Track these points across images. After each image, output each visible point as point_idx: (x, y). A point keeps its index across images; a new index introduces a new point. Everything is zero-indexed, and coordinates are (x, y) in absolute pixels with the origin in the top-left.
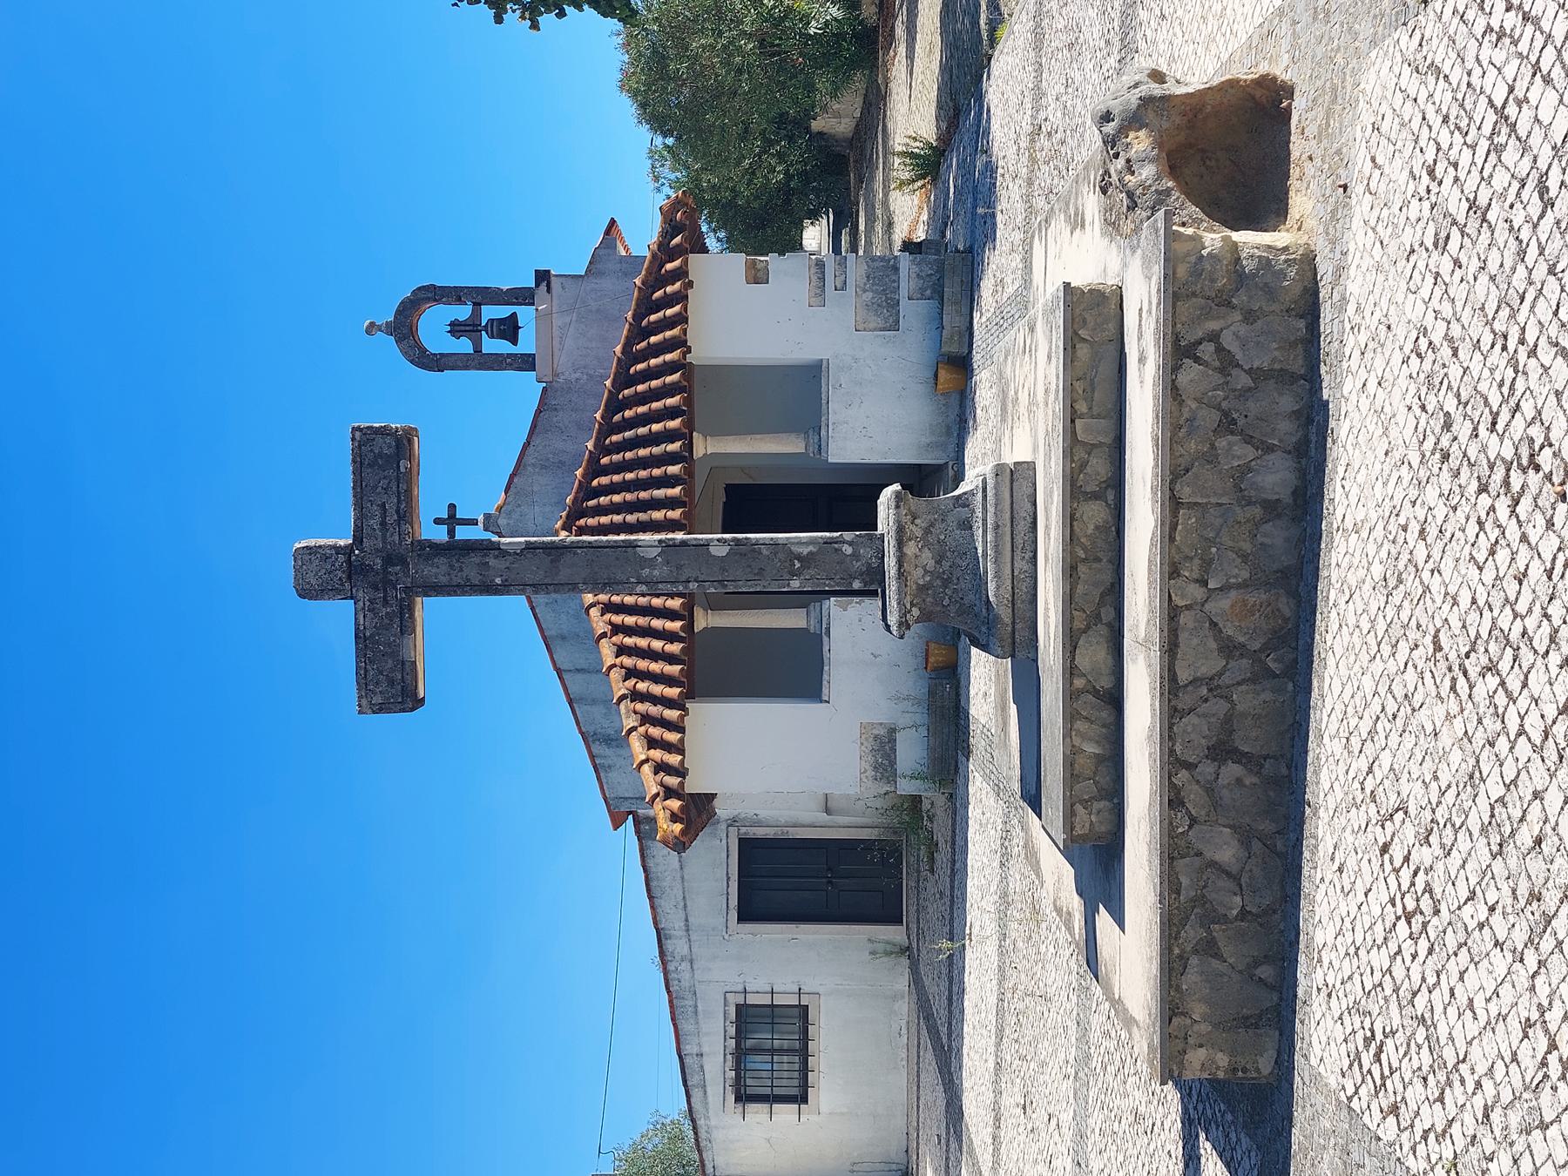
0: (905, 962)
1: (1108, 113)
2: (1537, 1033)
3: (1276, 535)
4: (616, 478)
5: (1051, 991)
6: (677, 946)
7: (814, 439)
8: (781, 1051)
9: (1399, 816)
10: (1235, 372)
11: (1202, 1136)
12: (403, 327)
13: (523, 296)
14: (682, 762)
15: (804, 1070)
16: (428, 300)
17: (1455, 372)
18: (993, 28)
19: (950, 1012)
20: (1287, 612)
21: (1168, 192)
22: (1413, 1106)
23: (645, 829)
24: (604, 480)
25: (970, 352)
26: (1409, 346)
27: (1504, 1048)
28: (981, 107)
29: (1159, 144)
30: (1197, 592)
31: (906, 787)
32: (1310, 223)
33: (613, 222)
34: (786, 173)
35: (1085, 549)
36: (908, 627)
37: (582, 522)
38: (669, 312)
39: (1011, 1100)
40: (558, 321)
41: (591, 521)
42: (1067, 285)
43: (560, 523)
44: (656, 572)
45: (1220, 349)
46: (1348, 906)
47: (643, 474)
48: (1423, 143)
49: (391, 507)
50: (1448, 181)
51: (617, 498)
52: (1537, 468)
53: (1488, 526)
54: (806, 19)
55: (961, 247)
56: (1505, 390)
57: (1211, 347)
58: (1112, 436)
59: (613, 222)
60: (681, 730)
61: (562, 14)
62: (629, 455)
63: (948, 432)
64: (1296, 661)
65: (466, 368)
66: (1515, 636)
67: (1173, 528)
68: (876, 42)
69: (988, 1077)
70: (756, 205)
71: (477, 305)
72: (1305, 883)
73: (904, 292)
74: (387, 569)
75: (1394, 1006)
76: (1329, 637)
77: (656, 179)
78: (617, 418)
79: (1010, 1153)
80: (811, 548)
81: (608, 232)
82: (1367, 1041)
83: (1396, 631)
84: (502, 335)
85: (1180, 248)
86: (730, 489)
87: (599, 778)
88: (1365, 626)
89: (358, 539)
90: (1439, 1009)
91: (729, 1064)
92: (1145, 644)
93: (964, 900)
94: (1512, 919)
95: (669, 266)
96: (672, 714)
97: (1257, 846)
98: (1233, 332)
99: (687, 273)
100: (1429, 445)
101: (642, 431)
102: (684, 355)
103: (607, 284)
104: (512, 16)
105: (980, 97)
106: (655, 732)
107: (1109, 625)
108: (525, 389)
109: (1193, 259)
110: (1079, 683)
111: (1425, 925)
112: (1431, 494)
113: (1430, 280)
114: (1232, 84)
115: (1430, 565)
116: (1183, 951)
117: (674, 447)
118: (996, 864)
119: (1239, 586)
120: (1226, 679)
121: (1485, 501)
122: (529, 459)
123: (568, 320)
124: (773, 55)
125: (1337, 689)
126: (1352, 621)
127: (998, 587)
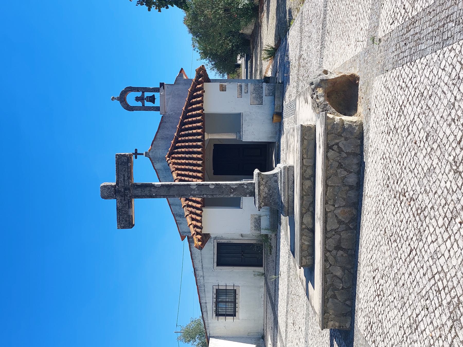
0: (263, 277)
1: (312, 83)
2: (402, 329)
3: (352, 194)
4: (183, 144)
5: (300, 295)
6: (200, 273)
7: (238, 135)
8: (228, 302)
9: (377, 271)
10: (342, 153)
11: (334, 340)
12: (122, 98)
13: (156, 90)
14: (201, 225)
15: (235, 307)
16: (129, 91)
17: (390, 167)
18: (290, 21)
19: (275, 294)
20: (355, 213)
21: (327, 105)
22: (378, 342)
23: (191, 240)
24: (180, 144)
25: (283, 111)
26: (381, 156)
27: (396, 331)
28: (286, 42)
29: (325, 92)
30: (332, 208)
31: (263, 232)
32: (362, 115)
33: (182, 69)
34: (232, 45)
35: (305, 192)
36: (261, 208)
37: (173, 156)
38: (198, 99)
39: (290, 321)
40: (166, 97)
41: (176, 156)
42: (301, 125)
43: (167, 156)
44: (195, 192)
45: (339, 147)
46: (366, 290)
47: (191, 144)
48: (386, 106)
49: (126, 175)
50: (390, 118)
51: (183, 150)
52: (405, 196)
53: (396, 206)
54: (238, 4)
55: (280, 82)
56: (400, 175)
57: (336, 147)
58: (313, 164)
59: (182, 69)
60: (201, 216)
61: (167, 8)
62: (187, 138)
63: (276, 134)
64: (357, 225)
65: (140, 110)
66: (400, 235)
67: (326, 192)
68: (258, 10)
69: (285, 314)
70: (223, 55)
71: (143, 92)
72: (357, 282)
73: (264, 94)
74: (125, 192)
75: (375, 317)
76: (364, 222)
77: (194, 47)
78: (183, 127)
79: (290, 335)
80: (236, 186)
81: (180, 72)
82: (370, 324)
83: (377, 226)
84: (150, 101)
85: (329, 121)
86: (215, 145)
87: (178, 227)
88: (371, 222)
89: (117, 183)
90: (384, 319)
91: (214, 305)
92: (320, 219)
93: (279, 264)
94: (398, 302)
95: (198, 86)
96: (198, 212)
97: (346, 271)
98: (342, 143)
99: (203, 89)
100: (385, 182)
101: (190, 132)
102: (202, 111)
103: (180, 87)
104: (153, 8)
105: (286, 39)
106: (194, 216)
107: (312, 212)
108: (156, 117)
109: (332, 124)
110: (304, 226)
111: (381, 298)
112: (385, 194)
113: (386, 141)
114: (344, 76)
115: (384, 212)
116: (328, 297)
117: (199, 137)
118: (287, 256)
119: (343, 207)
120: (339, 230)
121: (395, 200)
122: (158, 136)
123: (169, 97)
124: (229, 13)
125: (365, 236)
126: (368, 219)
127: (284, 198)
